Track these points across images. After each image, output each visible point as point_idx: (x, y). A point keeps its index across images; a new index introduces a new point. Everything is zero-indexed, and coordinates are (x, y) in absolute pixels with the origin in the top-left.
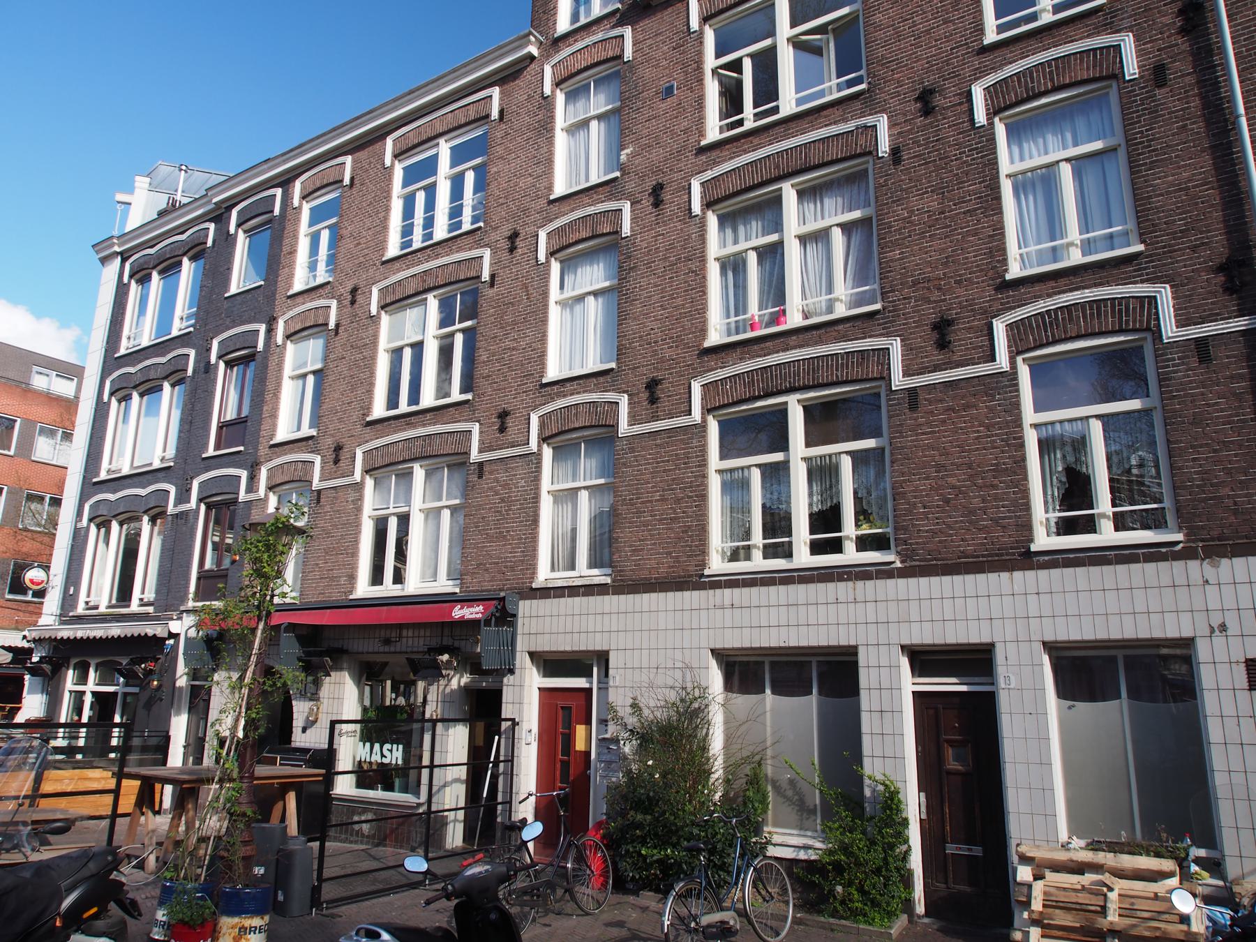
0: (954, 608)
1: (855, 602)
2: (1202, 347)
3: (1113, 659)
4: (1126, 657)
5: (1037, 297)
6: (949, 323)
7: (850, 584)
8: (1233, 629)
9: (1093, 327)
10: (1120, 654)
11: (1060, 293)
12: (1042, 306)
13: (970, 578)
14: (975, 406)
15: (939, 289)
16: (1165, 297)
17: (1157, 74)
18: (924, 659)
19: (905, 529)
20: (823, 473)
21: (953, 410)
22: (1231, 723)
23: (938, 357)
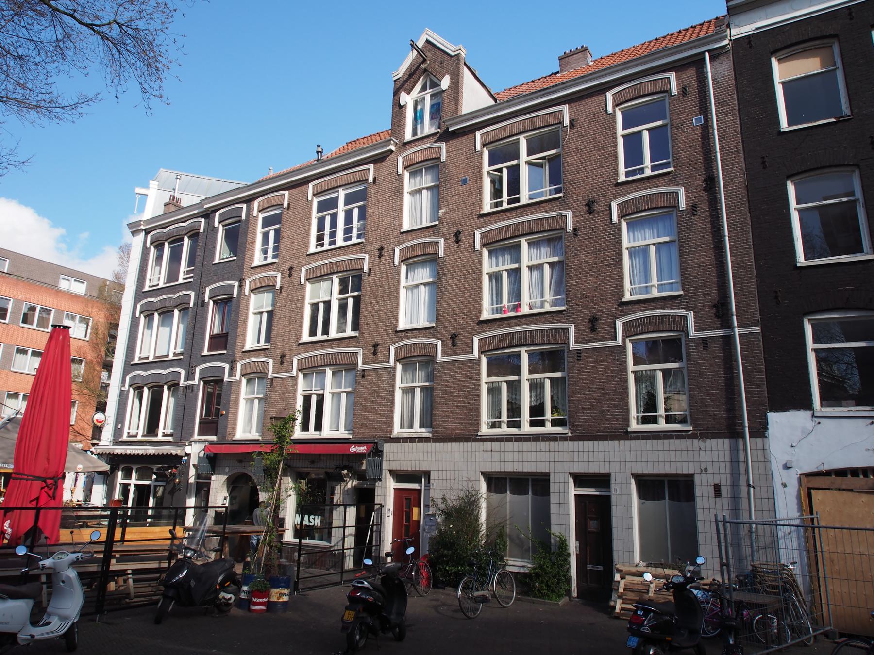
0: (594, 456)
3: (663, 481)
4: (669, 481)
5: (636, 311)
8: (710, 470)
13: (601, 442)
14: (607, 361)
20: (536, 387)
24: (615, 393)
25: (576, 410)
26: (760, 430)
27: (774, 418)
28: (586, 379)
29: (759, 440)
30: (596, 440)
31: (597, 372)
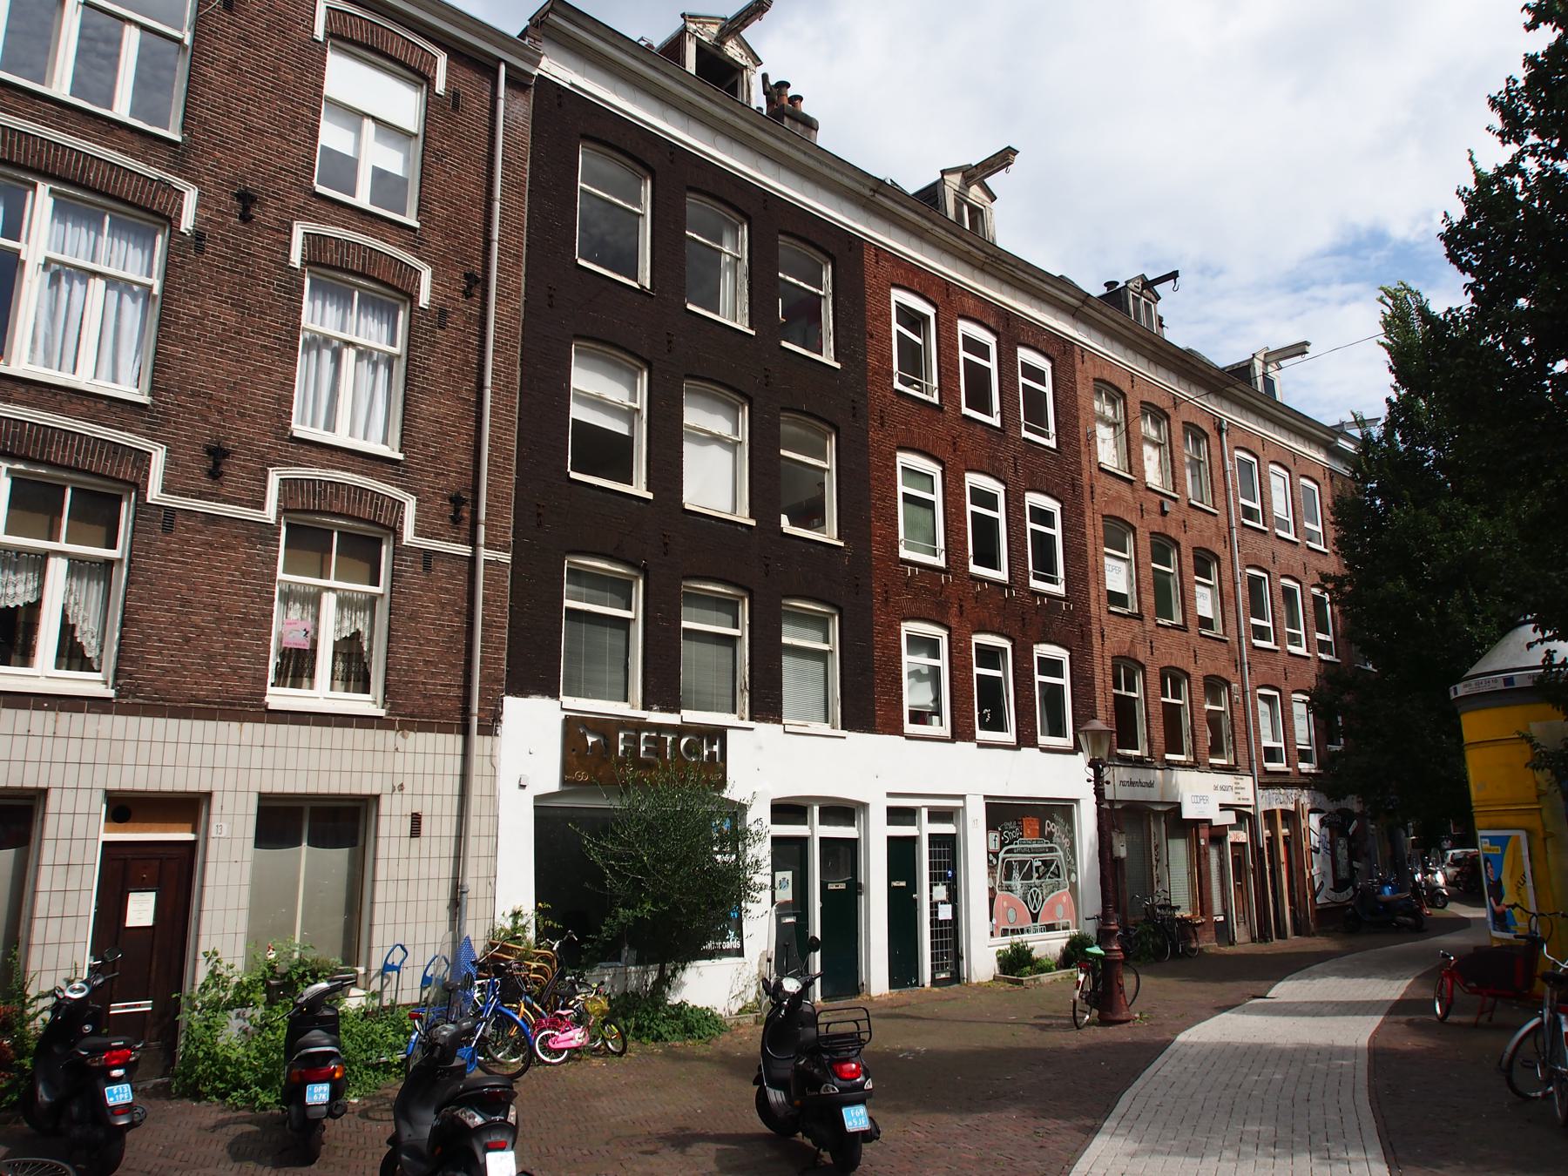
0: (164, 753)
1: (29, 734)
2: (428, 557)
3: (301, 809)
5: (312, 464)
6: (226, 454)
7: (51, 715)
8: (407, 790)
9: (118, 473)
10: (307, 806)
11: (333, 467)
12: (315, 473)
13: (198, 724)
14: (234, 549)
15: (220, 412)
16: (159, 458)
17: (440, 315)
18: (122, 807)
19: (133, 661)
21: (211, 546)
22: (393, 863)
23: (206, 484)
24: (245, 620)
25: (142, 644)
26: (491, 726)
27: (511, 704)
28: (180, 578)
29: (488, 739)
30: (145, 715)
31: (210, 568)
